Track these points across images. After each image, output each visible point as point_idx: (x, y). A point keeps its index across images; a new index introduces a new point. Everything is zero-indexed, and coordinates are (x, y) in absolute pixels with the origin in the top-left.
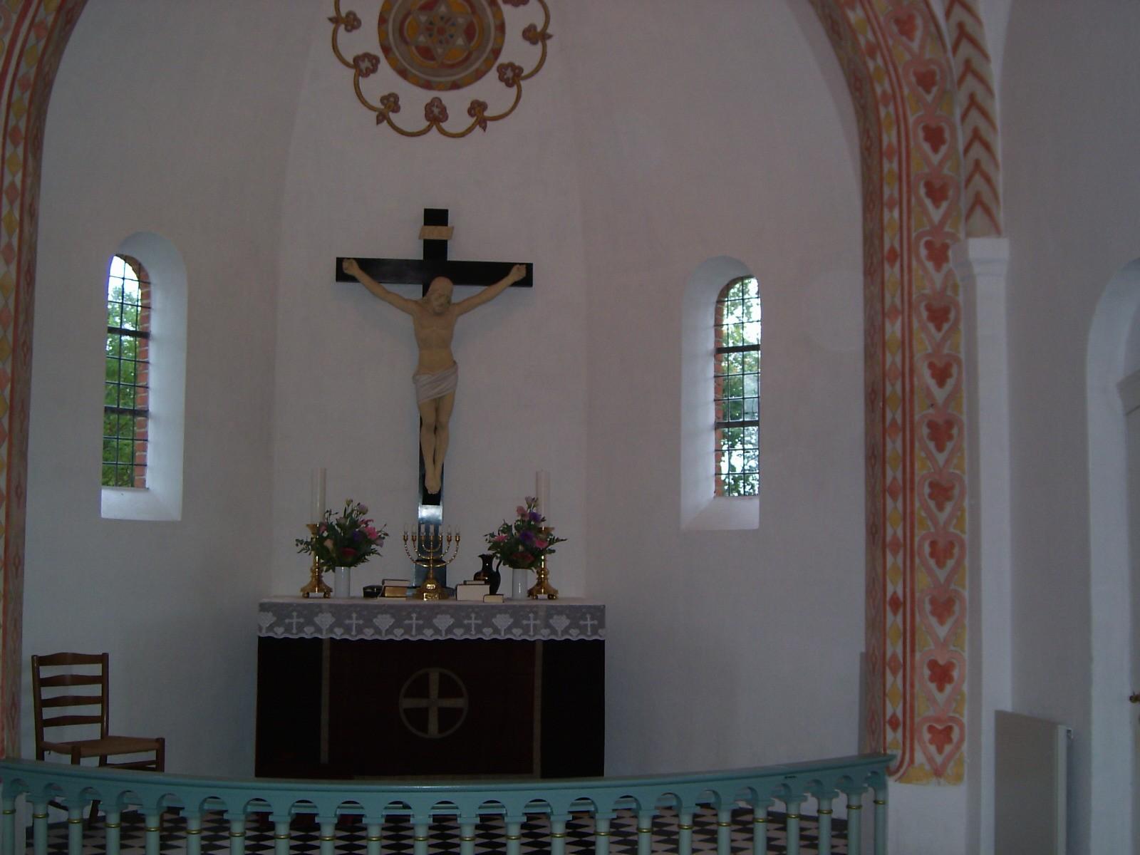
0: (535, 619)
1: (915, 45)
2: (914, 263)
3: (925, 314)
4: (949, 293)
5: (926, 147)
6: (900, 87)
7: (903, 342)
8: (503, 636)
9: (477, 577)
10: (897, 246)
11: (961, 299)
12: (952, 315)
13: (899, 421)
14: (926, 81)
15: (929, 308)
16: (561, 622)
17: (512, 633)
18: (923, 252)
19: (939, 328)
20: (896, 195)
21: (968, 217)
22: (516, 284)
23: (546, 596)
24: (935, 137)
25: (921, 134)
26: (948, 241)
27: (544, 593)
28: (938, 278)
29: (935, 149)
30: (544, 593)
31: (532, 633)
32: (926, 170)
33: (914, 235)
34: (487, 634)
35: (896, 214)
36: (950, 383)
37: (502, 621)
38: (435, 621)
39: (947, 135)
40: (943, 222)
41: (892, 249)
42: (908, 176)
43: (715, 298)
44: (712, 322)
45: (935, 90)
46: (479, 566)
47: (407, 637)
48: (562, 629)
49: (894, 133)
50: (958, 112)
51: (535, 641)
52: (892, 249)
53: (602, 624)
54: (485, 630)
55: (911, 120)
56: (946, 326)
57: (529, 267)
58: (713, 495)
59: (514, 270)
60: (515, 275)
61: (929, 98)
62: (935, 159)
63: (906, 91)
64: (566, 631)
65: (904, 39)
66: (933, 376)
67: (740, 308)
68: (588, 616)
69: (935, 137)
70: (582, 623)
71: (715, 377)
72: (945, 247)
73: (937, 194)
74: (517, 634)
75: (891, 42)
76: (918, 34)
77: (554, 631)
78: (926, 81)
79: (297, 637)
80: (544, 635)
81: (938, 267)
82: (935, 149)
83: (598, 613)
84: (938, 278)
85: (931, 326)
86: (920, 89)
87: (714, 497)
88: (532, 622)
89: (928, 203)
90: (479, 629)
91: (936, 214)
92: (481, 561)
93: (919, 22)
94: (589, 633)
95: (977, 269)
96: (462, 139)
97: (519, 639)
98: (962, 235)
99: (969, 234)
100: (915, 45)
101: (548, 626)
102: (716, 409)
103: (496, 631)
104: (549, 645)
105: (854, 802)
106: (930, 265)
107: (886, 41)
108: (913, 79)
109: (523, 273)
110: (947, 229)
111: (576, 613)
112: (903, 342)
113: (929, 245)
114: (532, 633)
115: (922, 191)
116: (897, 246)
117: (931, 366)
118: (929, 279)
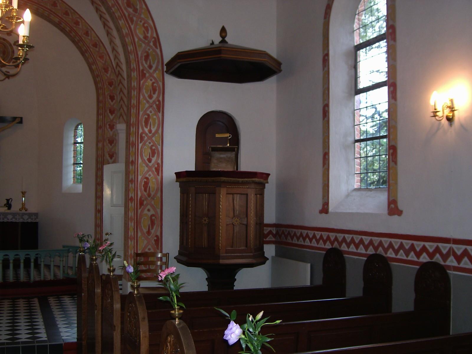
0: (19, 216)
1: (108, 75)
2: (105, 129)
3: (108, 142)
4: (114, 137)
5: (110, 101)
6: (104, 85)
7: (102, 148)
8: (10, 221)
9: (5, 205)
10: (102, 125)
11: (117, 138)
12: (115, 142)
13: (101, 168)
14: (111, 84)
15: (109, 140)
16: (26, 217)
17: (12, 220)
18: (108, 126)
19: (111, 145)
20: (102, 112)
21: (119, 118)
22: (18, 123)
23: (25, 210)
24: (112, 98)
25: (109, 97)
26: (114, 124)
27: (24, 210)
28: (111, 133)
29: (112, 101)
30: (24, 210)
31: (18, 220)
32: (110, 106)
33: (105, 122)
34: (6, 220)
35: (102, 117)
36: (113, 158)
37: (10, 217)
38: (7, 217)
39: (115, 98)
40: (113, 119)
41: (100, 126)
42: (105, 108)
43: (74, 128)
44: (73, 135)
45: (113, 86)
46: (5, 202)
47: (32, 221)
48: (26, 219)
49: (102, 97)
50: (118, 93)
51: (18, 222)
52: (100, 126)
53: (37, 218)
54: (5, 219)
55: (106, 94)
56: (113, 145)
57: (21, 118)
58: (72, 183)
59: (17, 119)
60: (17, 121)
61: (111, 88)
62: (112, 104)
63: (105, 87)
64: (27, 219)
65: (106, 73)
66: (109, 157)
67: (371, 29)
68: (33, 215)
69: (112, 98)
70: (32, 217)
71: (74, 150)
72: (113, 125)
73: (112, 112)
74: (14, 220)
75: (102, 74)
76: (109, 72)
77: (24, 220)
78: (111, 84)
79: (18, 221)
80: (21, 220)
81: (112, 130)
82: (112, 101)
83: (36, 215)
84: (111, 133)
85: (109, 145)
86: (109, 86)
87: (73, 184)
88: (18, 217)
89: (110, 114)
90: (3, 219)
91: (111, 117)
92: (6, 201)
93: (110, 69)
94: (34, 220)
95: (119, 131)
96: (3, 82)
97: (14, 221)
98: (118, 122)
99: (119, 123)
100: (108, 75)
101: (22, 218)
102: (74, 159)
103: (8, 219)
104: (23, 223)
105: (62, 259)
106: (109, 130)
107: (101, 74)
108: (107, 84)
109: (20, 120)
110: (114, 121)
111: (30, 215)
112: (102, 148)
113: (109, 125)
114: (18, 220)
115: (108, 111)
116: (102, 125)
117: (109, 154)
118: (109, 133)
